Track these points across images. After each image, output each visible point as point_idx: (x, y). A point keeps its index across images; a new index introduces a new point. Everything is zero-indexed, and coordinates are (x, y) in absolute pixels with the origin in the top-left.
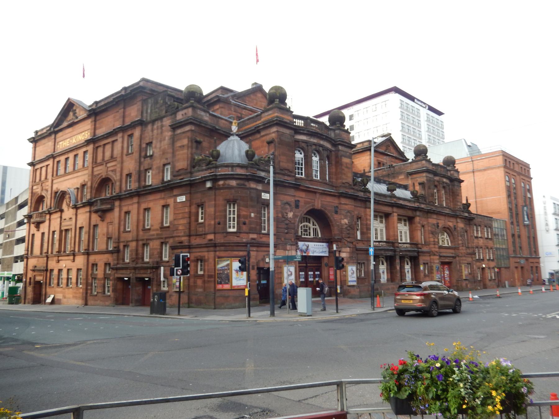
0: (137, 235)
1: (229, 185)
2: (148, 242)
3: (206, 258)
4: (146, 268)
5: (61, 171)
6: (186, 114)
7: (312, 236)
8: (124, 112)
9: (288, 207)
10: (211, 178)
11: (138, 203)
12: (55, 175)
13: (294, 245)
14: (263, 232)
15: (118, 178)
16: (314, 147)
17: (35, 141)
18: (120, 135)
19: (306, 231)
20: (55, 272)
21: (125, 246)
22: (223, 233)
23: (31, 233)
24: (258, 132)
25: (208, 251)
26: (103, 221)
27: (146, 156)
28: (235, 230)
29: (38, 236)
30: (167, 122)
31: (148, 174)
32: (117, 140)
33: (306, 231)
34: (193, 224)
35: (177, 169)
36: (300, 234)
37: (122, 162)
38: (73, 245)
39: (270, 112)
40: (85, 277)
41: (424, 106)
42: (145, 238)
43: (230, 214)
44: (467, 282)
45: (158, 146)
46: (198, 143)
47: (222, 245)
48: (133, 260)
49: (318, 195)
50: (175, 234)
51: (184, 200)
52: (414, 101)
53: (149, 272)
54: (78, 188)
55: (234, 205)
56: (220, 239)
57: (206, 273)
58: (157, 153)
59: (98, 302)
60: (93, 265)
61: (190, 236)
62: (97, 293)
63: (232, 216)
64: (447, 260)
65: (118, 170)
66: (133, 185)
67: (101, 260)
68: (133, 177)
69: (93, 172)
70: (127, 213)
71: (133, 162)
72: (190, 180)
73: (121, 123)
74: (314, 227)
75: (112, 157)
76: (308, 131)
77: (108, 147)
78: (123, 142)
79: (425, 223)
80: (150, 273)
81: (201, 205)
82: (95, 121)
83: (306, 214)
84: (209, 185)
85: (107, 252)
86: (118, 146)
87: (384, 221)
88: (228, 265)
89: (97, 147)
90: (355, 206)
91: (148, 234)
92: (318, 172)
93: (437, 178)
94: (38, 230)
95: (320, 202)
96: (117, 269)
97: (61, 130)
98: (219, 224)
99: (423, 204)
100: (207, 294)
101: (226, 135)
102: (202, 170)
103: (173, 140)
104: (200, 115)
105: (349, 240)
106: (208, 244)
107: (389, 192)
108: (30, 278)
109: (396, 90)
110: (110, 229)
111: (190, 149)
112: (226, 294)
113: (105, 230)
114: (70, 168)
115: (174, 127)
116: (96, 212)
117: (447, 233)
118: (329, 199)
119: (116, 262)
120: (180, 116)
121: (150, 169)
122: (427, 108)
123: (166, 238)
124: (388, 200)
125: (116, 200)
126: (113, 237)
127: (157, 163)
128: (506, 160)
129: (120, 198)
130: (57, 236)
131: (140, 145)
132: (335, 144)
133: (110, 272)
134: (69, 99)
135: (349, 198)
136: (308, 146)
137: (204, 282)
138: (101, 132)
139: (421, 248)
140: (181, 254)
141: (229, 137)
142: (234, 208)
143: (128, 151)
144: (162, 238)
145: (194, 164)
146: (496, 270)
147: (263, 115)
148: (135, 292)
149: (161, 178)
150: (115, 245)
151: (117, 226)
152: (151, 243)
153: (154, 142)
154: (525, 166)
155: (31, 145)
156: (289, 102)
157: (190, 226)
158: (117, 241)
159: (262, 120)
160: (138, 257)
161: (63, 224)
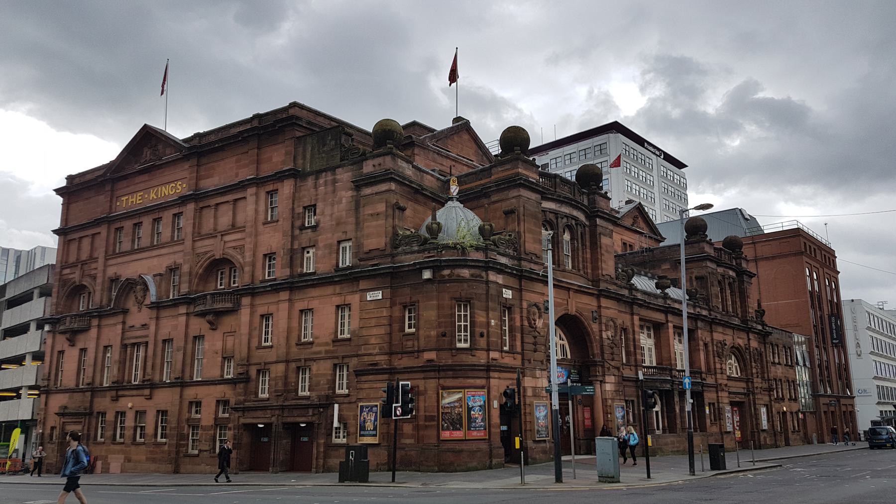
0: (288, 354)
1: (459, 276)
2: (308, 363)
3: (422, 388)
4: (307, 407)
6: (380, 165)
10: (431, 265)
11: (290, 300)
13: (544, 370)
15: (248, 259)
18: (251, 191)
20: (110, 417)
21: (259, 371)
22: (451, 349)
24: (487, 195)
27: (303, 228)
28: (467, 345)
31: (306, 255)
35: (366, 249)
39: (507, 167)
41: (658, 153)
42: (302, 357)
44: (765, 434)
45: (328, 211)
48: (276, 394)
50: (363, 352)
51: (380, 297)
52: (643, 146)
53: (311, 414)
54: (160, 275)
55: (465, 306)
56: (447, 359)
57: (422, 413)
59: (202, 467)
61: (391, 354)
62: (200, 451)
63: (463, 324)
64: (737, 399)
65: (248, 247)
66: (280, 272)
67: (209, 396)
68: (278, 259)
69: (193, 249)
70: (266, 317)
72: (394, 268)
76: (560, 196)
78: (257, 203)
80: (314, 415)
84: (427, 275)
85: (223, 382)
88: (460, 400)
91: (308, 351)
94: (73, 345)
96: (245, 410)
97: (125, 178)
98: (444, 335)
102: (412, 252)
103: (357, 205)
104: (403, 168)
106: (427, 366)
107: (659, 291)
108: (53, 428)
109: (616, 127)
111: (390, 220)
112: (458, 447)
113: (219, 345)
115: (359, 184)
116: (202, 314)
117: (735, 356)
118: (585, 299)
120: (368, 167)
124: (660, 302)
125: (242, 295)
126: (237, 356)
129: (252, 291)
130: (114, 355)
133: (227, 415)
134: (146, 127)
137: (417, 428)
138: (210, 183)
140: (401, 383)
144: (337, 358)
145: (396, 241)
146: (801, 416)
147: (494, 170)
149: (335, 262)
150: (240, 370)
151: (245, 339)
152: (315, 367)
153: (320, 206)
154: (829, 253)
155: (60, 200)
157: (391, 338)
159: (493, 177)
160: (287, 388)
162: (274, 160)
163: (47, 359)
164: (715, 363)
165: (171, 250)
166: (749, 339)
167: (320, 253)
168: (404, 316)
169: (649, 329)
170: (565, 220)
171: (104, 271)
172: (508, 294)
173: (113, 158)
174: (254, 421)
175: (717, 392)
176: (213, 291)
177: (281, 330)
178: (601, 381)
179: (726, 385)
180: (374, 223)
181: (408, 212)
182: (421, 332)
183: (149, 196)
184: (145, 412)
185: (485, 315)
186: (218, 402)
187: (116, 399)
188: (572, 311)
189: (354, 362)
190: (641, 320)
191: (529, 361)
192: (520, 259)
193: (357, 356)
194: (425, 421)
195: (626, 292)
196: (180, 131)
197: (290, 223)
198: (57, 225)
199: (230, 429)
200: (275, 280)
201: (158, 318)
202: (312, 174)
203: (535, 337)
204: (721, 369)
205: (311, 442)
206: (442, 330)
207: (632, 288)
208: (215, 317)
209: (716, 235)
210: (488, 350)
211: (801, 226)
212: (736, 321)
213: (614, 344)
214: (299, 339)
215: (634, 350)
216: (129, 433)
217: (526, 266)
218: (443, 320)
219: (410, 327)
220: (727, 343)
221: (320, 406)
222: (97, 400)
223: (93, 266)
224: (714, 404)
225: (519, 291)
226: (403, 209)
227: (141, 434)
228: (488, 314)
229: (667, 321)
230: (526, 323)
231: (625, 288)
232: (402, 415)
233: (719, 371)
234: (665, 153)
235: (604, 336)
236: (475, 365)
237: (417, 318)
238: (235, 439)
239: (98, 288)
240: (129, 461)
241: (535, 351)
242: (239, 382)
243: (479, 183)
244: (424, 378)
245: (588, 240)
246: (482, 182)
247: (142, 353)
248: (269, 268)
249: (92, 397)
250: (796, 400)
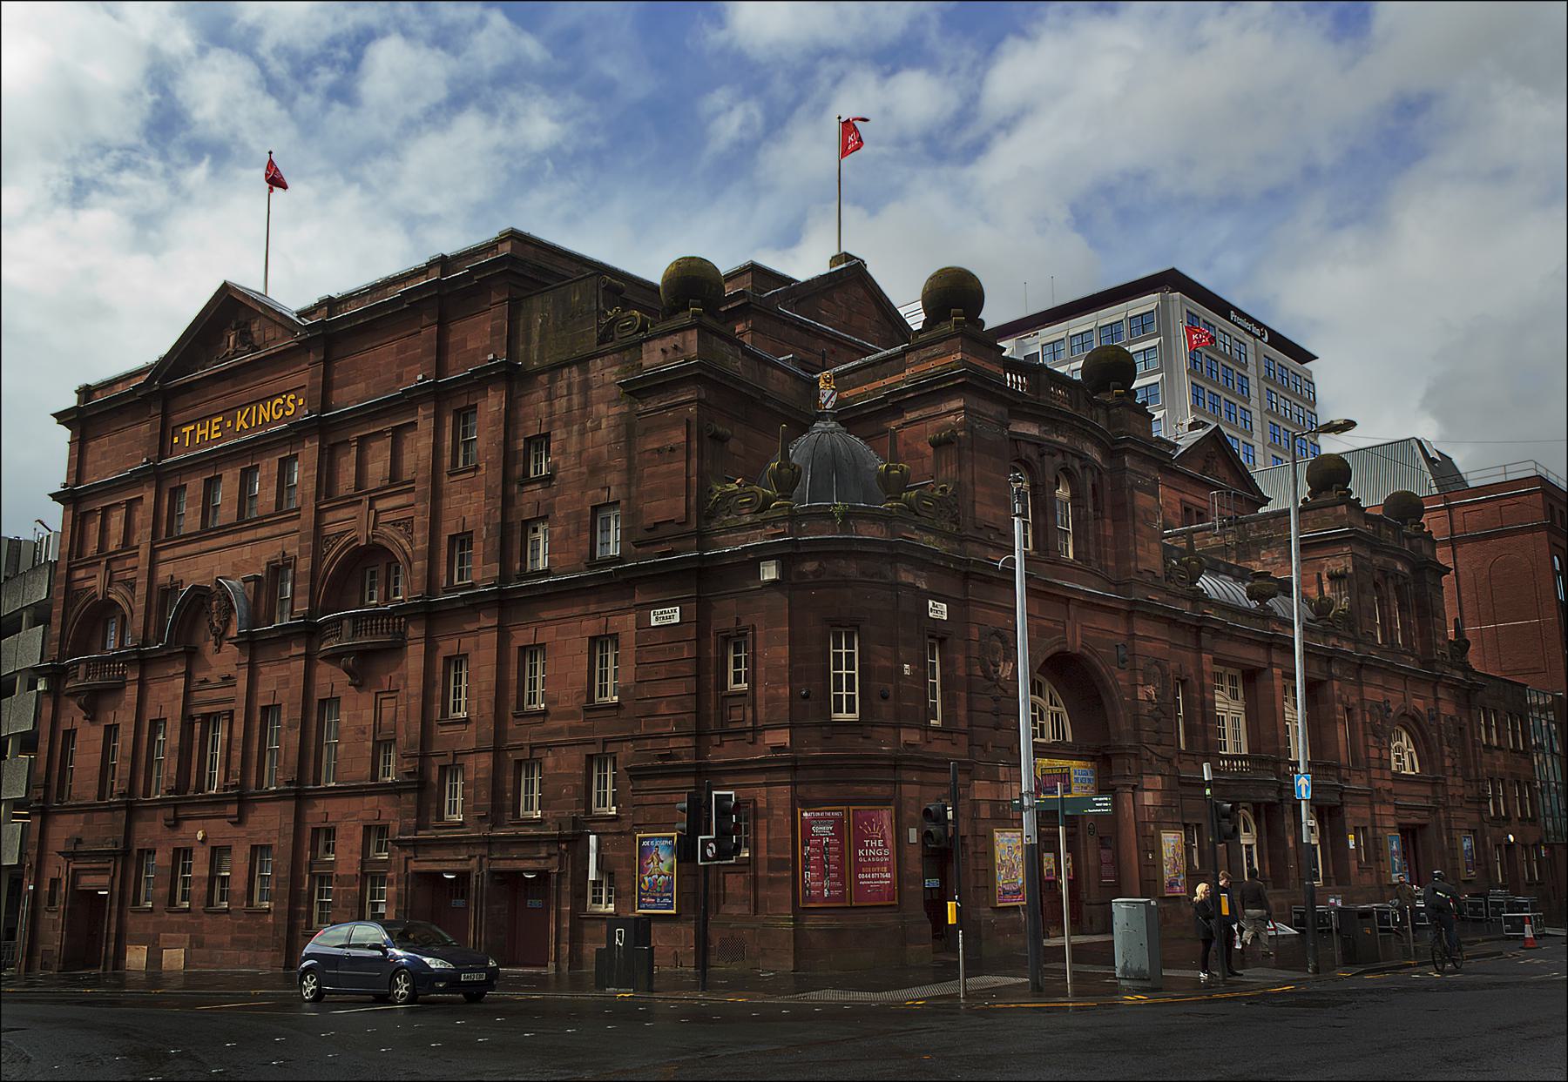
3: (762, 804)
4: (455, 843)
5: (190, 519)
6: (676, 347)
12: (166, 533)
15: (421, 545)
20: (162, 858)
21: (443, 768)
23: (65, 724)
26: (359, 686)
28: (855, 716)
29: (89, 739)
30: (606, 373)
32: (414, 424)
35: (647, 522)
37: (436, 495)
38: (236, 766)
40: (284, 874)
41: (1257, 332)
45: (573, 447)
46: (719, 439)
47: (818, 763)
51: (677, 620)
54: (257, 579)
57: (762, 854)
58: (569, 468)
60: (316, 831)
64: (1414, 820)
65: (421, 520)
66: (481, 572)
68: (478, 545)
69: (318, 526)
70: (456, 661)
71: (479, 497)
74: (1053, 708)
79: (1354, 700)
80: (549, 856)
82: (328, 363)
84: (769, 572)
86: (418, 449)
87: (1241, 694)
90: (1172, 645)
93: (1378, 560)
96: (417, 845)
99: (1347, 639)
103: (629, 431)
105: (1158, 750)
107: (1253, 604)
109: (1171, 280)
110: (387, 713)
113: (368, 715)
114: (227, 512)
115: (636, 390)
116: (334, 657)
117: (1409, 733)
118: (1102, 622)
120: (653, 356)
121: (544, 519)
122: (1266, 339)
123: (606, 742)
126: (402, 739)
128: (1551, 507)
130: (170, 737)
132: (1113, 452)
133: (385, 856)
134: (226, 288)
135: (1158, 618)
137: (755, 882)
138: (350, 397)
139: (1346, 780)
142: (850, 646)
143: (455, 462)
151: (416, 703)
153: (558, 434)
155: (65, 434)
158: (417, 751)
161: (198, 696)
162: (471, 345)
163: (43, 746)
164: (1367, 746)
165: (276, 530)
166: (1437, 700)
167: (558, 530)
169: (1233, 680)
170: (1059, 459)
172: (939, 610)
173: (164, 350)
174: (435, 867)
175: (1372, 807)
176: (350, 609)
177: (484, 687)
178: (1134, 787)
179: (1389, 791)
180: (663, 468)
181: (733, 445)
182: (760, 691)
183: (234, 423)
184: (228, 849)
186: (367, 829)
187: (175, 823)
188: (1075, 644)
190: (1216, 661)
191: (984, 747)
193: (633, 739)
194: (770, 869)
195: (1186, 607)
196: (294, 290)
197: (500, 470)
199: (391, 883)
200: (472, 586)
202: (542, 372)
203: (996, 700)
204: (1380, 758)
205: (546, 910)
207: (1199, 597)
208: (364, 665)
209: (1369, 493)
210: (897, 727)
211: (1542, 472)
212: (1410, 664)
213: (1165, 710)
214: (591, 698)
215: (1204, 724)
216: (199, 890)
217: (975, 552)
219: (737, 680)
220: (1394, 708)
221: (559, 839)
222: (140, 826)
223: (129, 563)
224: (1364, 829)
227: (222, 892)
229: (1271, 664)
231: (1183, 597)
232: (717, 856)
233: (1375, 763)
234: (1271, 332)
235: (1141, 696)
236: (869, 757)
237: (753, 663)
238: (399, 902)
239: (140, 606)
240: (201, 945)
242: (406, 791)
243: (881, 383)
244: (766, 784)
245: (1107, 504)
246: (887, 381)
247: (222, 735)
248: (461, 563)
250: (1533, 820)
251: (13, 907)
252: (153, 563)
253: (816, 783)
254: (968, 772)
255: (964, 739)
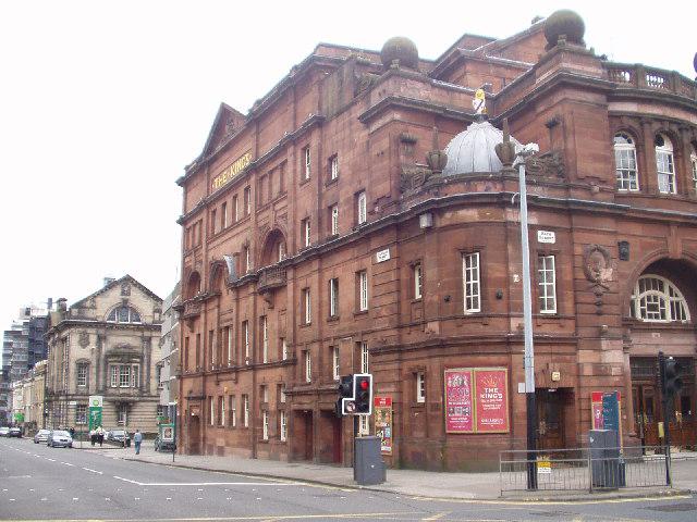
0: (321, 332)
4: (305, 394)
5: (217, 230)
6: (384, 91)
7: (669, 319)
8: (295, 110)
9: (598, 255)
11: (320, 270)
14: (546, 311)
16: (656, 126)
17: (183, 182)
18: (291, 150)
19: (652, 308)
21: (304, 352)
22: (456, 318)
25: (430, 357)
29: (193, 339)
33: (652, 308)
34: (405, 305)
36: (639, 316)
37: (296, 199)
43: (475, 285)
49: (674, 230)
51: (388, 257)
54: (237, 254)
61: (400, 327)
66: (309, 240)
67: (272, 376)
69: (257, 222)
73: (291, 125)
74: (674, 299)
75: (282, 192)
77: (277, 176)
78: (295, 163)
81: (415, 266)
83: (646, 271)
84: (424, 222)
89: (262, 178)
92: (674, 179)
95: (679, 242)
98: (447, 300)
100: (429, 444)
101: (462, 121)
110: (284, 322)
116: (262, 292)
119: (291, 382)
127: (346, 193)
129: (292, 265)
131: (320, 163)
136: (642, 124)
138: (266, 150)
141: (469, 124)
145: (403, 183)
148: (323, 432)
151: (291, 316)
155: (181, 189)
156: (586, 38)
160: (323, 371)
168: (413, 279)
171: (206, 256)
180: (380, 165)
185: (503, 269)
189: (370, 341)
192: (567, 188)
198: (179, 213)
201: (237, 300)
206: (445, 293)
218: (445, 279)
225: (566, 234)
226: (411, 142)
228: (507, 267)
230: (581, 275)
241: (599, 314)
249: (204, 382)
251: (388, 520)
252: (207, 251)
253: (453, 355)
254: (575, 344)
255: (571, 323)
